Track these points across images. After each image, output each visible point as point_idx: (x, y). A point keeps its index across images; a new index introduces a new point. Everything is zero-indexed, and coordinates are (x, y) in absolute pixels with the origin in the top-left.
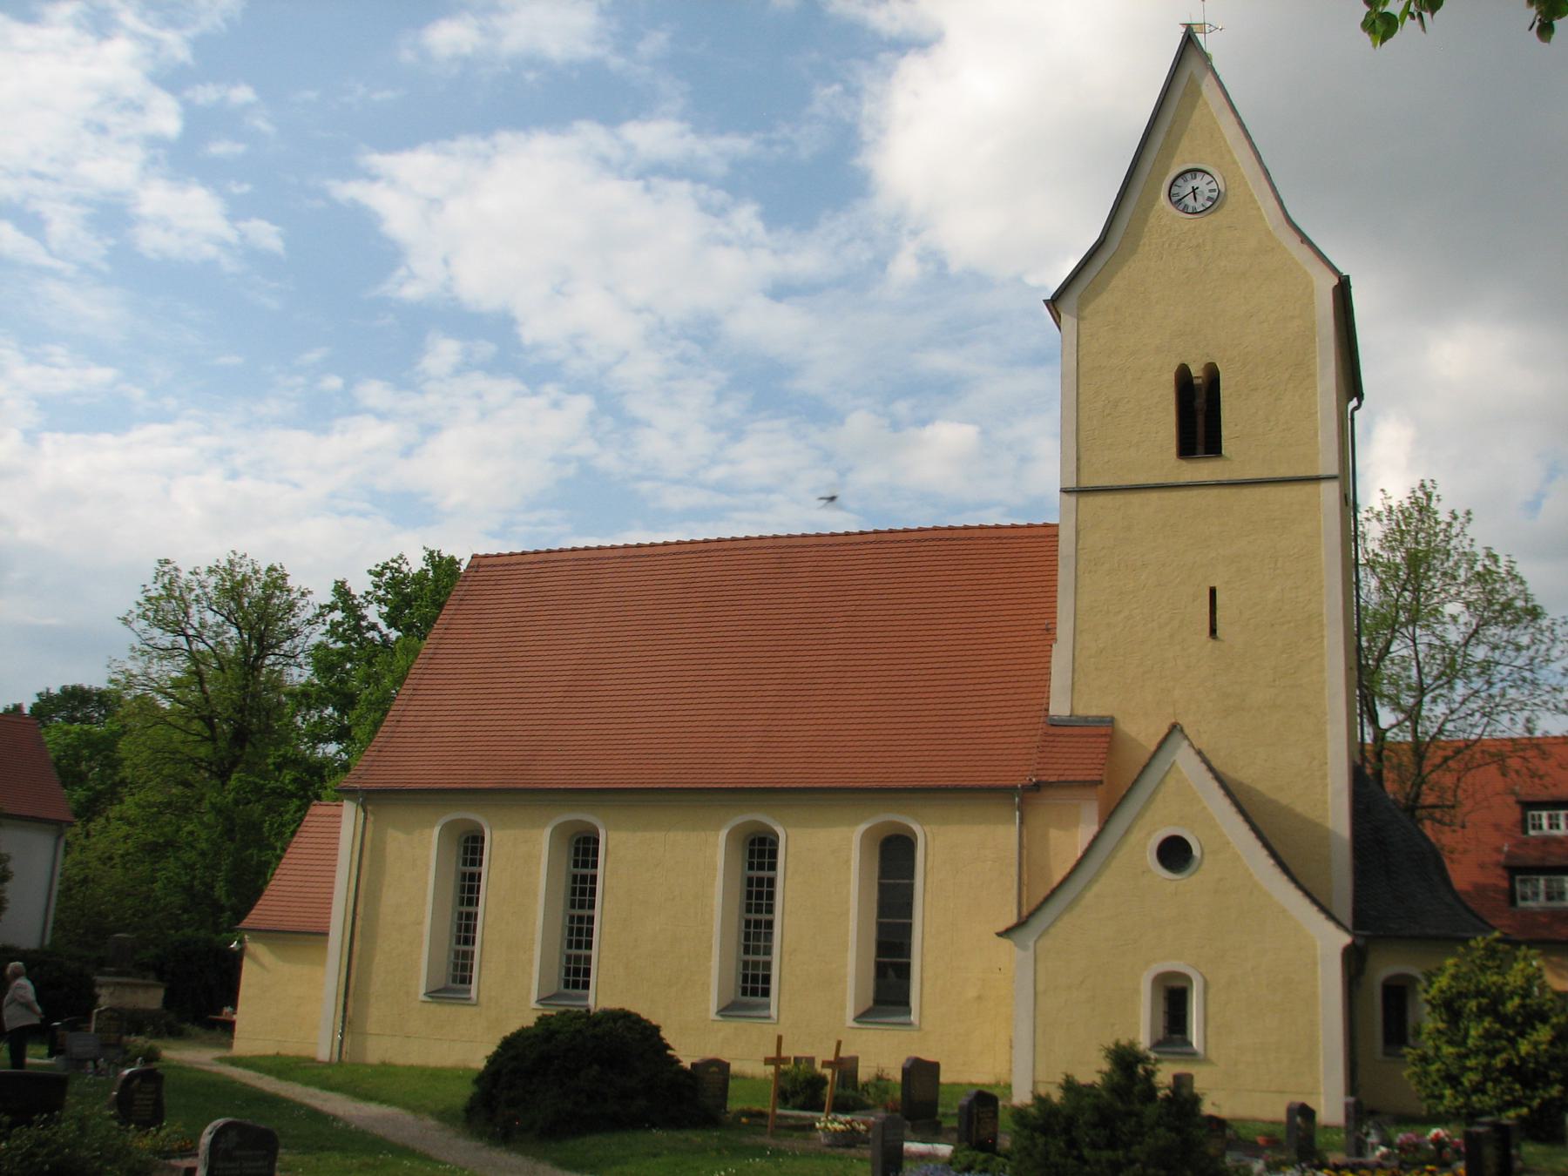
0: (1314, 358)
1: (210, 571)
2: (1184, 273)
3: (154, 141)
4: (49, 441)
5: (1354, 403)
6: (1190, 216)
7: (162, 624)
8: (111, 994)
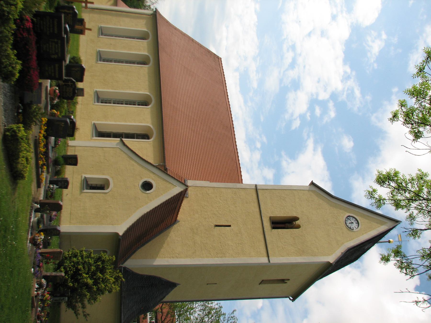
2: (327, 219)
3: (317, 94)
4: (237, 74)
5: (291, 298)
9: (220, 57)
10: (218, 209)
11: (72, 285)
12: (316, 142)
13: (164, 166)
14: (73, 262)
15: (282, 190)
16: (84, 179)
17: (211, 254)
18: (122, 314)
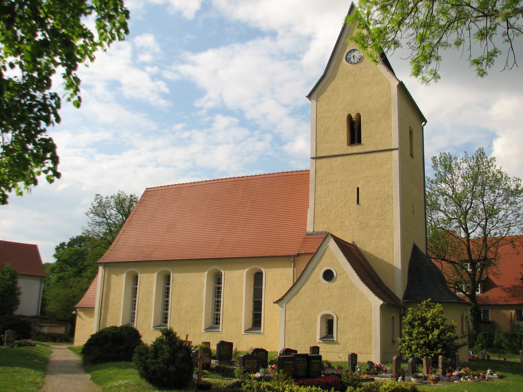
0: (391, 109)
1: (112, 197)
4: (98, 157)
5: (424, 123)
6: (352, 65)
7: (98, 215)
8: (48, 329)
9: (144, 190)
10: (340, 200)
11: (440, 349)
12: (183, 62)
13: (295, 256)
14: (416, 349)
15: (317, 130)
16: (322, 340)
17: (389, 210)
18: (449, 301)
